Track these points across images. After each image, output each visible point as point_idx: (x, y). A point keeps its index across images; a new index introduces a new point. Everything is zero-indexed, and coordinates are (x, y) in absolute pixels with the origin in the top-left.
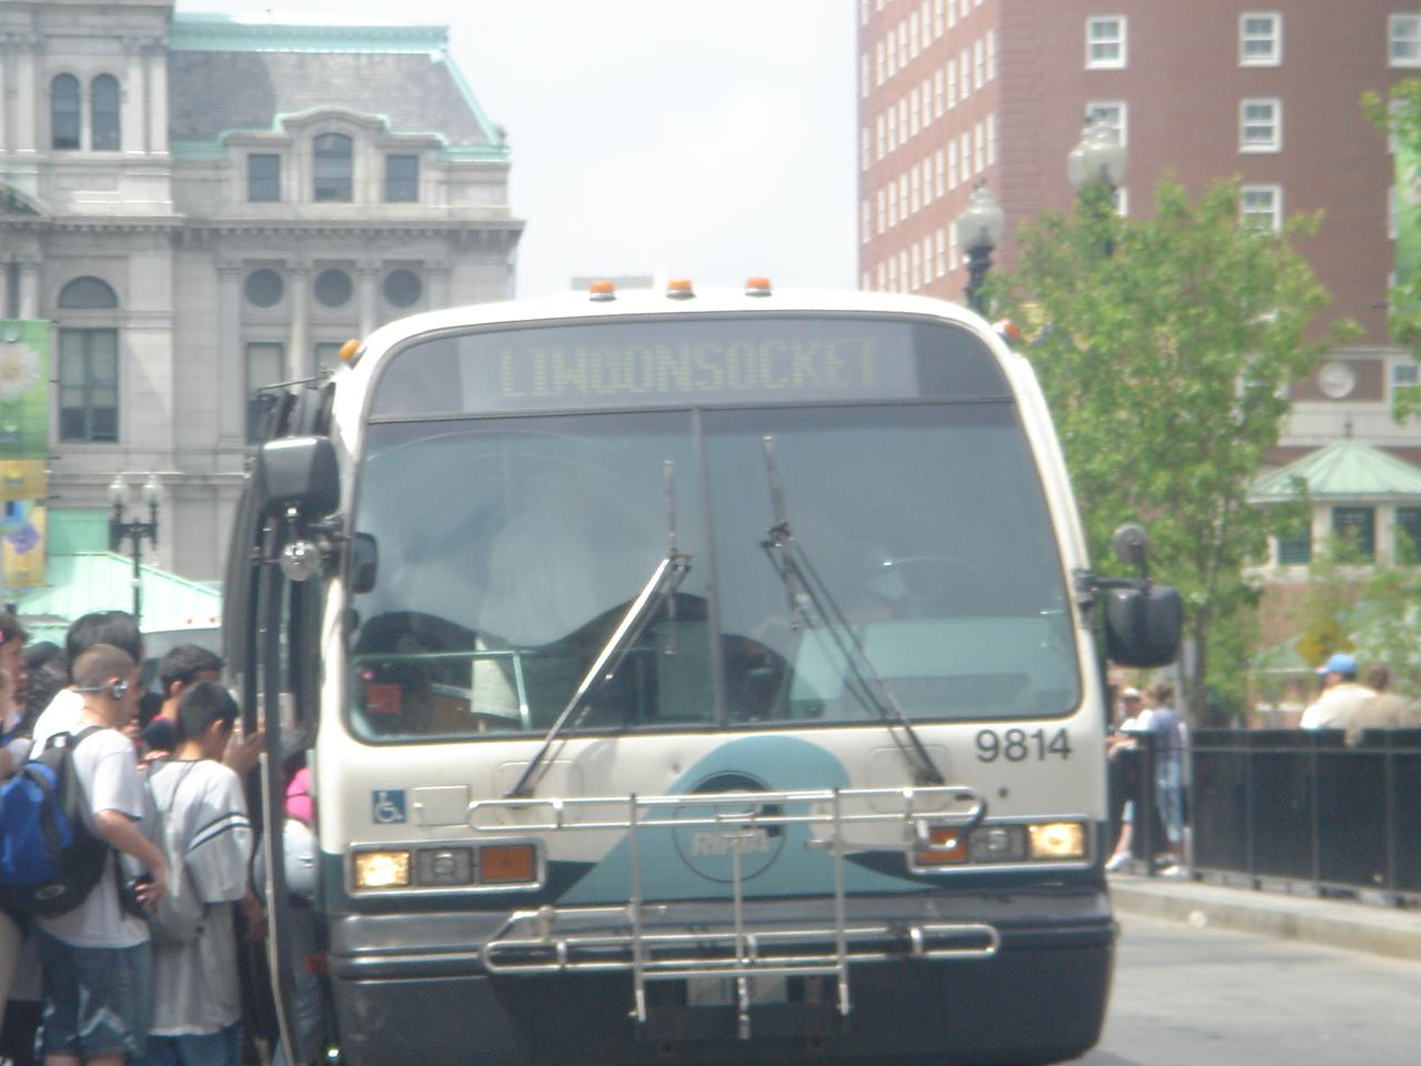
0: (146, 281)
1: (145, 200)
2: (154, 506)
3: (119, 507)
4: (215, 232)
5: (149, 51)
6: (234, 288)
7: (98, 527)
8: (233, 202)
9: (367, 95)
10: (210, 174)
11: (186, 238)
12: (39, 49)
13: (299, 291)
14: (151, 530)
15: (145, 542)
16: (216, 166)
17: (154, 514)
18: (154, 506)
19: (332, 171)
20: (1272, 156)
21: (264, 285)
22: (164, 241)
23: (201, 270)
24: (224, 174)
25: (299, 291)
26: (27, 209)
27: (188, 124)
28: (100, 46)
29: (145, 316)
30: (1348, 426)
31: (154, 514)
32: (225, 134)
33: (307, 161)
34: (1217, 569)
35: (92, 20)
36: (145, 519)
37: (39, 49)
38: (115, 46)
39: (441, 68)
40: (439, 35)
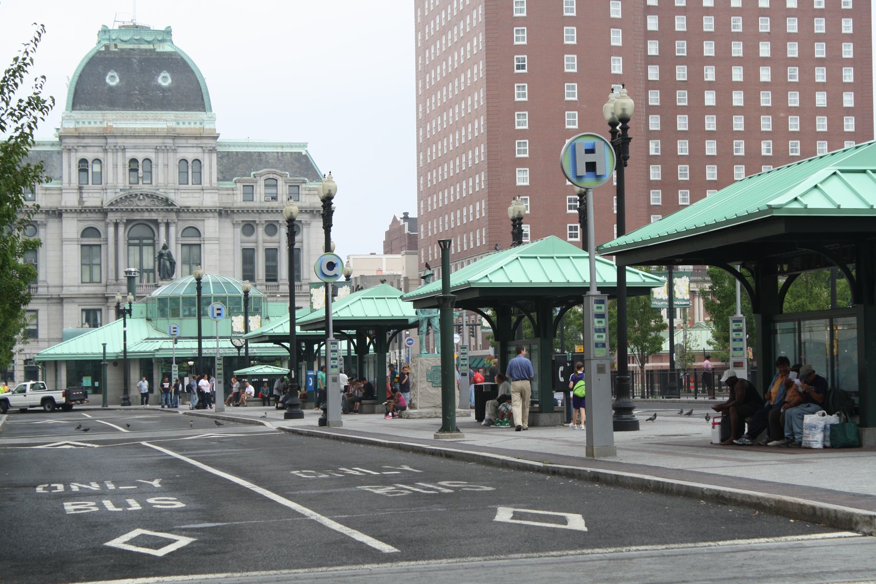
0: (210, 227)
1: (210, 200)
2: (130, 303)
3: (118, 303)
4: (233, 212)
5: (212, 150)
6: (239, 230)
7: (113, 313)
8: (238, 200)
9: (281, 166)
10: (230, 192)
11: (223, 213)
12: (174, 151)
13: (260, 230)
14: (130, 311)
15: (128, 316)
16: (233, 189)
17: (130, 306)
18: (130, 303)
19: (272, 191)
20: (683, 7)
21: (249, 228)
22: (216, 214)
23: (227, 223)
24: (235, 192)
25: (260, 230)
26: (172, 204)
27: (225, 175)
28: (195, 150)
29: (210, 239)
30: (20, 392)
31: (130, 306)
32: (235, 179)
33: (263, 187)
34: (718, 408)
35: (192, 142)
36: (127, 307)
37: (174, 151)
38: (200, 150)
39: (306, 157)
40: (305, 145)
